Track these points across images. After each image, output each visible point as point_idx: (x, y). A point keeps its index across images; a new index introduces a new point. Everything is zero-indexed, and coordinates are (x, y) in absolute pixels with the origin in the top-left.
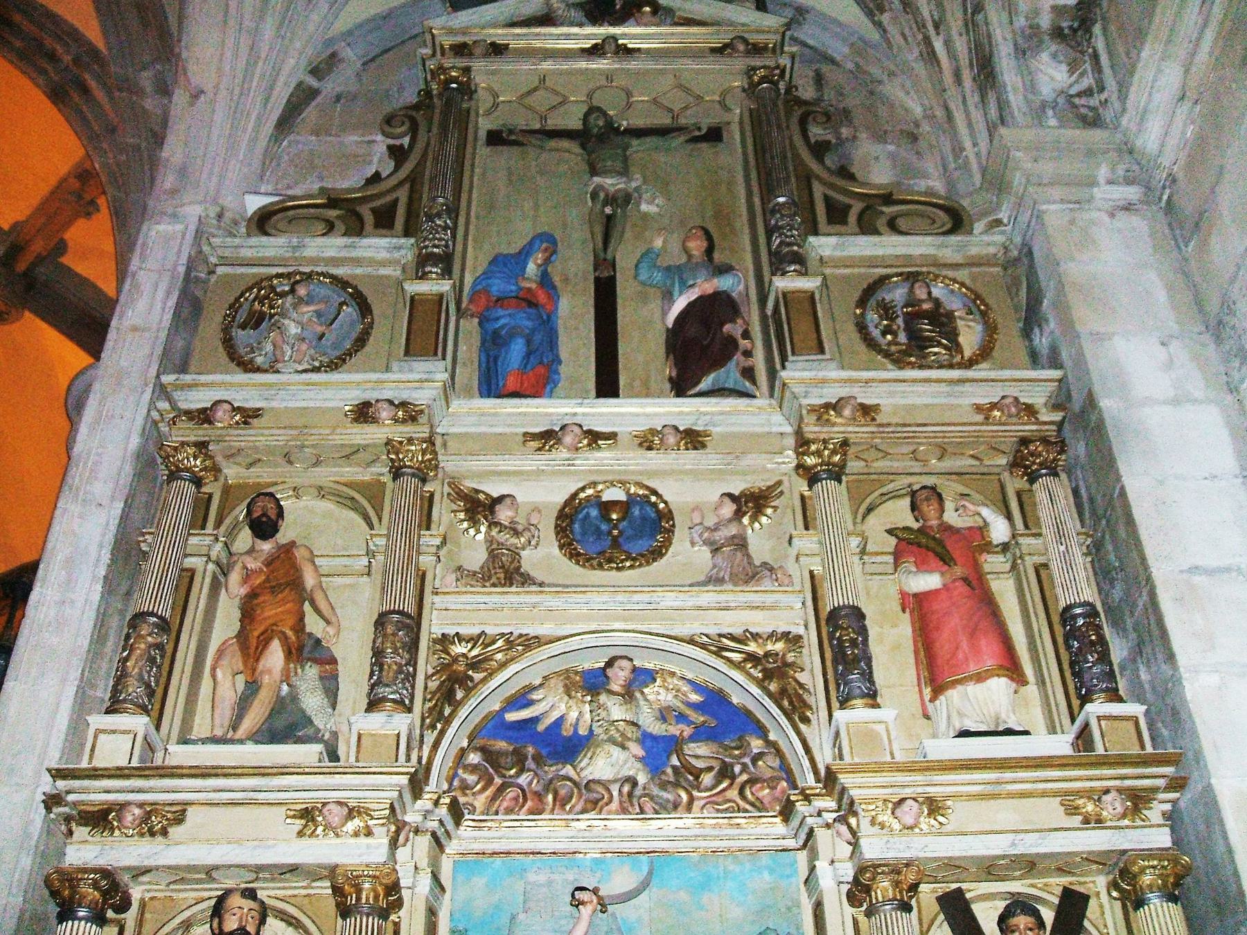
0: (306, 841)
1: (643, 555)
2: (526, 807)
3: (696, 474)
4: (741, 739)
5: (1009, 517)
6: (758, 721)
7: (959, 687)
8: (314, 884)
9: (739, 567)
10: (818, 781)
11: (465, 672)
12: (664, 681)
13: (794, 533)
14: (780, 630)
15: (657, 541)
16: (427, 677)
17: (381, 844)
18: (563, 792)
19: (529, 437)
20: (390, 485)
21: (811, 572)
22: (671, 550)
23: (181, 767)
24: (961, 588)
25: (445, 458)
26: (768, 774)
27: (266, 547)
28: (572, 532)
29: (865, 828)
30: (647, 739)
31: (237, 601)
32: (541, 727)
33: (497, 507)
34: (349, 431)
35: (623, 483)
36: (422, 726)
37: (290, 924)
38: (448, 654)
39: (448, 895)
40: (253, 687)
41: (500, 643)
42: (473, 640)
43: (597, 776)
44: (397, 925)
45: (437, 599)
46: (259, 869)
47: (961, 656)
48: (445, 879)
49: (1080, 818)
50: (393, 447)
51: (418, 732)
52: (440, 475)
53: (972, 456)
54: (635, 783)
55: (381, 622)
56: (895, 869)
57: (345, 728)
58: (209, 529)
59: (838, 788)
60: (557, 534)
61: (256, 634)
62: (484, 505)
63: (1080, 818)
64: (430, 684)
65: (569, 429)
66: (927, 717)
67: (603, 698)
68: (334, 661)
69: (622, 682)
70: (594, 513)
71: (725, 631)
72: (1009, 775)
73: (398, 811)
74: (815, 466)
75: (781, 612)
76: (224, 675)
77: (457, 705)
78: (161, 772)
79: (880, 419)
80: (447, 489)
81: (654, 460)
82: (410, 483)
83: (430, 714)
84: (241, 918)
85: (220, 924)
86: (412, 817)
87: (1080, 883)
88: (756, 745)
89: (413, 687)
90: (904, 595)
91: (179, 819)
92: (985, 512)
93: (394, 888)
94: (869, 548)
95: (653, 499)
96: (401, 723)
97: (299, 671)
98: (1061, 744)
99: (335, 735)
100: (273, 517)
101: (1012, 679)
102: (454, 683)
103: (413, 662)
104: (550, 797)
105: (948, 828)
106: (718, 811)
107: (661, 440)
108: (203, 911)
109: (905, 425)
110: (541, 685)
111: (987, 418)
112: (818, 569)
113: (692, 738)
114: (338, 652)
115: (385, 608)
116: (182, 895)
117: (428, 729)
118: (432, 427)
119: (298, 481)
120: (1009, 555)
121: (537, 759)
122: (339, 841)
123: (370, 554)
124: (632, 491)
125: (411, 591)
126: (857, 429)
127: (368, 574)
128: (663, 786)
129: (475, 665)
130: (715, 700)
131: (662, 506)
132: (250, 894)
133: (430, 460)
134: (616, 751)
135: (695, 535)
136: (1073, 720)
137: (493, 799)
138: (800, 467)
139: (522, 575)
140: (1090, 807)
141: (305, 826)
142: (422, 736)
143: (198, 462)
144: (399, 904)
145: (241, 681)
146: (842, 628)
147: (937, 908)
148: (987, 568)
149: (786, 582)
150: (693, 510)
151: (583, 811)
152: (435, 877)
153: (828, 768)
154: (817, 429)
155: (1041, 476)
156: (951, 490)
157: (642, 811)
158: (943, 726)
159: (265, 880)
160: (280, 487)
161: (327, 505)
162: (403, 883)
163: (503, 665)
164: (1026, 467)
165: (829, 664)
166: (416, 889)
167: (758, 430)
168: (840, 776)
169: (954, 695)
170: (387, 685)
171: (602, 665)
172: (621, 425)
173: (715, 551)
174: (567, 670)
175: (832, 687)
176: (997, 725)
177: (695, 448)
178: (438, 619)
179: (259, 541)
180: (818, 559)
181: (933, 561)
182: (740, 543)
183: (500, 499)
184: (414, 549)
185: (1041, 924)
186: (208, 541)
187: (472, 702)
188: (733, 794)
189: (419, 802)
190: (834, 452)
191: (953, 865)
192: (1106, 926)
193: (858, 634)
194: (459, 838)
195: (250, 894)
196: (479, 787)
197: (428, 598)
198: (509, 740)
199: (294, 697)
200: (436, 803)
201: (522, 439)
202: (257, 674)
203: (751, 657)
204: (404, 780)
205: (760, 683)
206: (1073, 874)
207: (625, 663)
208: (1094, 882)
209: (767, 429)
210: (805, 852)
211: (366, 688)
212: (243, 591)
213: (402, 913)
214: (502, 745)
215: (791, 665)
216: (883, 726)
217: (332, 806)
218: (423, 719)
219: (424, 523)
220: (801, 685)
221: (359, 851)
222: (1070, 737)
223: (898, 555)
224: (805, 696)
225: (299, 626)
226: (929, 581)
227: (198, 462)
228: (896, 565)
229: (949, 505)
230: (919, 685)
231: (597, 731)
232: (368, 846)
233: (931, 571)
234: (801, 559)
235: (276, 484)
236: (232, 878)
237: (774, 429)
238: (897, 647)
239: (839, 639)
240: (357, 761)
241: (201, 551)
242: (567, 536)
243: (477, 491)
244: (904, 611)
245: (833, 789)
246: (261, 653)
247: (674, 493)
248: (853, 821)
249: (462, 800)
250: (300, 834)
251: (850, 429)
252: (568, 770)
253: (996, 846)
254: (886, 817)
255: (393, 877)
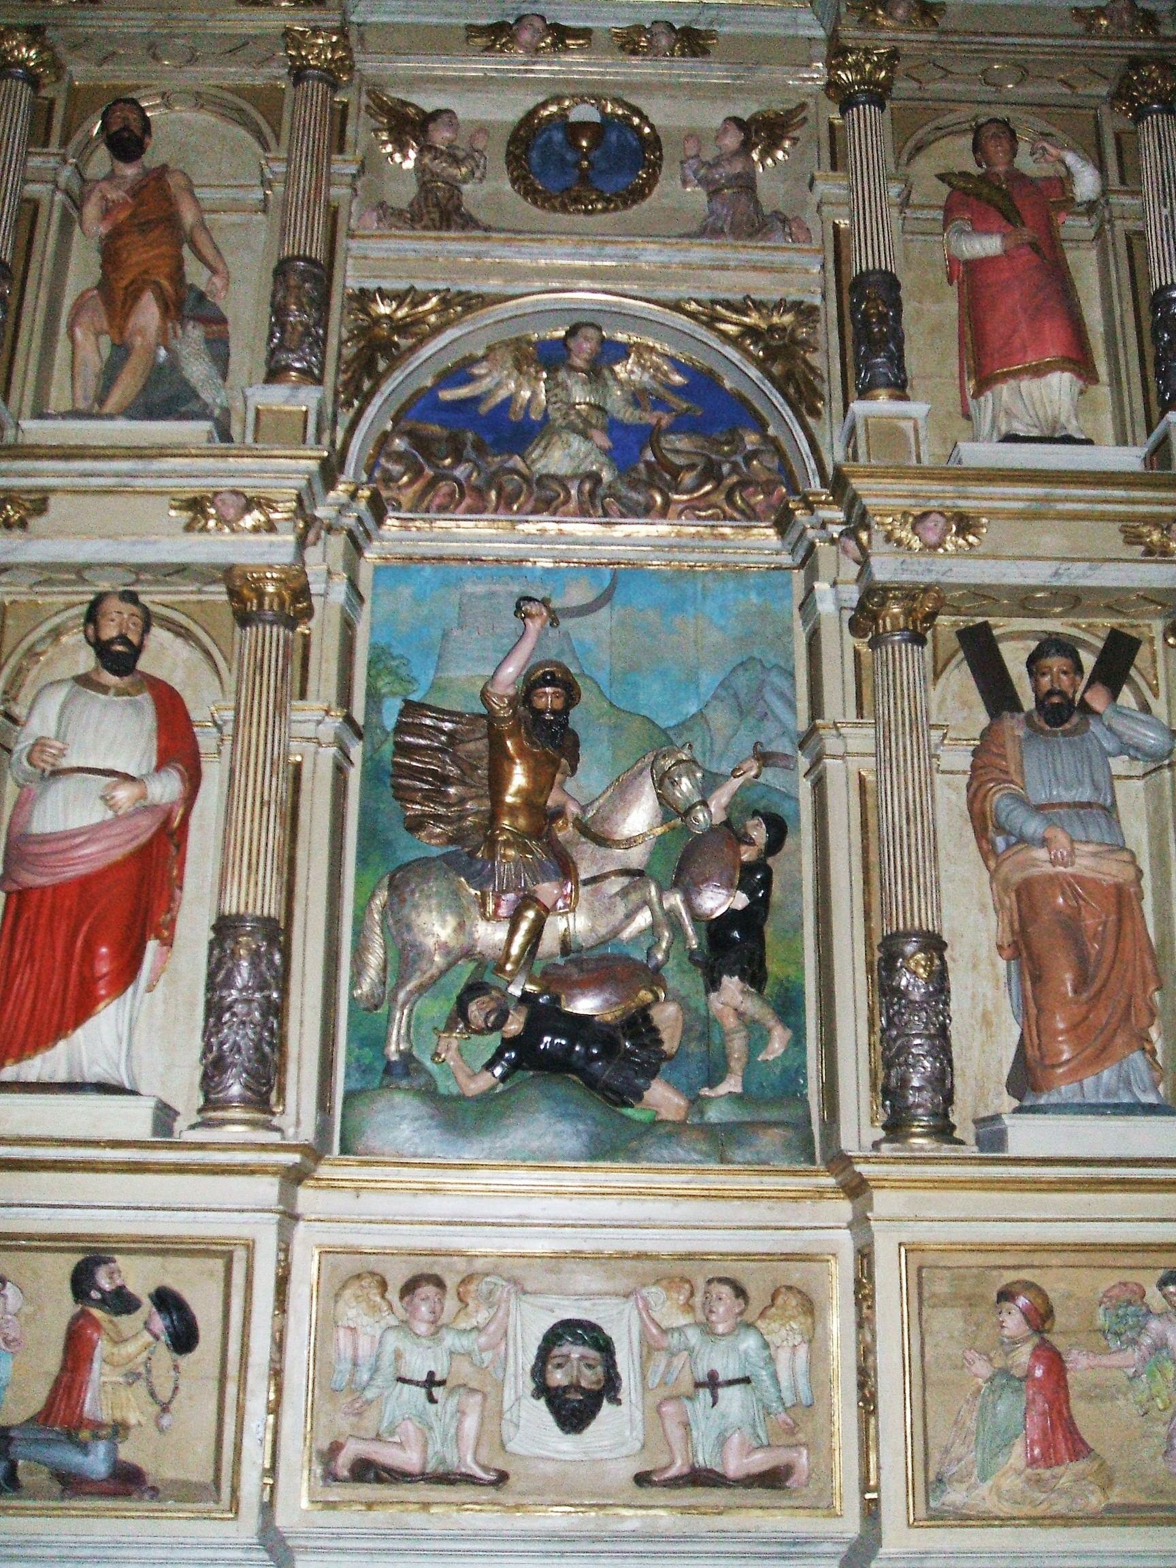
0: (195, 537)
1: (619, 196)
2: (464, 505)
3: (694, 91)
4: (733, 431)
5: (1101, 167)
6: (756, 411)
7: (1012, 382)
8: (206, 589)
9: (743, 215)
10: (824, 484)
11: (389, 338)
12: (640, 356)
13: (817, 174)
14: (791, 298)
15: (640, 177)
16: (342, 343)
17: (285, 543)
18: (509, 488)
19: (473, 31)
20: (290, 92)
21: (836, 226)
22: (656, 190)
23: (38, 446)
24: (1026, 255)
25: (362, 57)
26: (763, 476)
27: (130, 171)
28: (528, 161)
29: (878, 546)
30: (614, 427)
31: (94, 243)
32: (484, 409)
33: (431, 126)
34: (232, 16)
35: (598, 98)
36: (335, 401)
37: (178, 634)
38: (368, 315)
39: (367, 607)
40: (122, 350)
41: (434, 300)
42: (399, 297)
43: (552, 470)
44: (306, 638)
45: (353, 244)
46: (140, 569)
47: (1017, 342)
48: (365, 587)
49: (1142, 548)
50: (293, 39)
51: (330, 410)
52: (356, 81)
53: (1064, 82)
54: (595, 478)
55: (282, 270)
56: (910, 594)
57: (239, 404)
58: (54, 148)
59: (849, 494)
60: (509, 163)
61: (124, 283)
62: (412, 122)
63: (1142, 548)
64: (345, 351)
65: (526, 22)
66: (967, 416)
67: (562, 375)
68: (223, 321)
69: (586, 356)
70: (558, 136)
71: (722, 296)
72: (1059, 491)
73: (306, 503)
74: (852, 84)
75: (793, 275)
76: (85, 335)
77: (378, 379)
78: (16, 452)
79: (944, 23)
80: (365, 99)
81: (639, 69)
82: (315, 89)
83: (346, 389)
84: (121, 625)
85: (97, 630)
86: (321, 512)
87: (1132, 626)
88: (751, 440)
89: (324, 353)
90: (952, 260)
91: (40, 507)
92: (1070, 158)
93: (303, 592)
94: (915, 198)
95: (636, 121)
96: (308, 398)
97: (180, 332)
98: (1130, 459)
99: (227, 411)
100: (138, 132)
101: (1079, 376)
102: (375, 351)
103: (323, 322)
104: (493, 494)
105: (981, 550)
106: (699, 518)
107: (649, 41)
108: (77, 616)
109: (976, 34)
110: (485, 358)
111: (1088, 29)
112: (844, 223)
113: (673, 429)
114: (229, 314)
115: (287, 251)
116: (49, 599)
117: (343, 405)
118: (344, 13)
119: (168, 85)
120: (1094, 219)
121: (479, 447)
122: (234, 537)
123: (266, 183)
124: (609, 109)
125: (319, 230)
126: (912, 37)
127: (264, 211)
128: (634, 485)
129: (402, 328)
130: (702, 382)
131: (647, 130)
132: (131, 597)
133: (341, 59)
134: (576, 442)
135: (689, 172)
136: (1150, 430)
137: (423, 494)
138: (832, 87)
139: (462, 215)
140: (1156, 537)
141: (194, 519)
142: (335, 415)
143: (32, 53)
144: (308, 613)
145: (105, 341)
146: (868, 299)
147: (956, 644)
148: (1064, 233)
149: (802, 237)
150: (686, 139)
151: (535, 512)
152: (353, 584)
153: (837, 469)
154: (858, 33)
155: (1151, 113)
156: (1027, 127)
157: (606, 514)
158: (986, 428)
159: (150, 583)
160: (143, 92)
161: (205, 118)
162: (315, 588)
163: (437, 330)
164: (1133, 100)
165: (849, 343)
166: (329, 595)
167: (781, 31)
168: (853, 481)
169: (1005, 390)
170: (292, 351)
171: (561, 333)
172: (597, 19)
173: (714, 193)
174: (517, 339)
175: (851, 373)
176: (1054, 429)
177: (694, 55)
178: (356, 269)
179: (120, 165)
180: (846, 210)
181: (995, 218)
182: (747, 184)
183: (438, 114)
184: (323, 178)
185: (1078, 668)
186: (53, 162)
187: (398, 376)
188: (720, 498)
189: (332, 494)
190: (878, 67)
191: (980, 594)
192: (1156, 677)
193: (890, 307)
194: (381, 539)
195: (131, 597)
196: (405, 479)
197: (342, 241)
198: (442, 423)
199: (174, 364)
200: (353, 496)
201: (463, 33)
202: (127, 334)
203: (751, 332)
204: (313, 465)
205: (760, 364)
206: (1126, 615)
207: (591, 332)
208: (1149, 626)
209: (791, 32)
210: (802, 572)
211: (263, 354)
212: (103, 229)
213: (313, 623)
214: (435, 429)
215: (805, 344)
216: (911, 423)
217: (226, 497)
218: (336, 394)
219: (336, 143)
220: (812, 369)
221: (261, 549)
222: (1142, 451)
223: (949, 211)
224: (817, 382)
225: (178, 274)
226: (988, 245)
227: (32, 53)
228: (946, 223)
229: (1024, 147)
230: (961, 378)
231: (555, 415)
232: (271, 544)
233: (988, 232)
234: (825, 209)
235: (138, 87)
236: (107, 579)
237: (802, 32)
238: (936, 329)
239: (865, 314)
240: (256, 441)
241: (47, 174)
242: (522, 167)
243: (405, 104)
244: (950, 282)
245: (843, 495)
246: (131, 307)
247: (661, 113)
248: (864, 536)
249: (385, 494)
250: (189, 528)
251: (902, 36)
252: (516, 461)
253: (1036, 574)
254: (904, 534)
255: (302, 579)
